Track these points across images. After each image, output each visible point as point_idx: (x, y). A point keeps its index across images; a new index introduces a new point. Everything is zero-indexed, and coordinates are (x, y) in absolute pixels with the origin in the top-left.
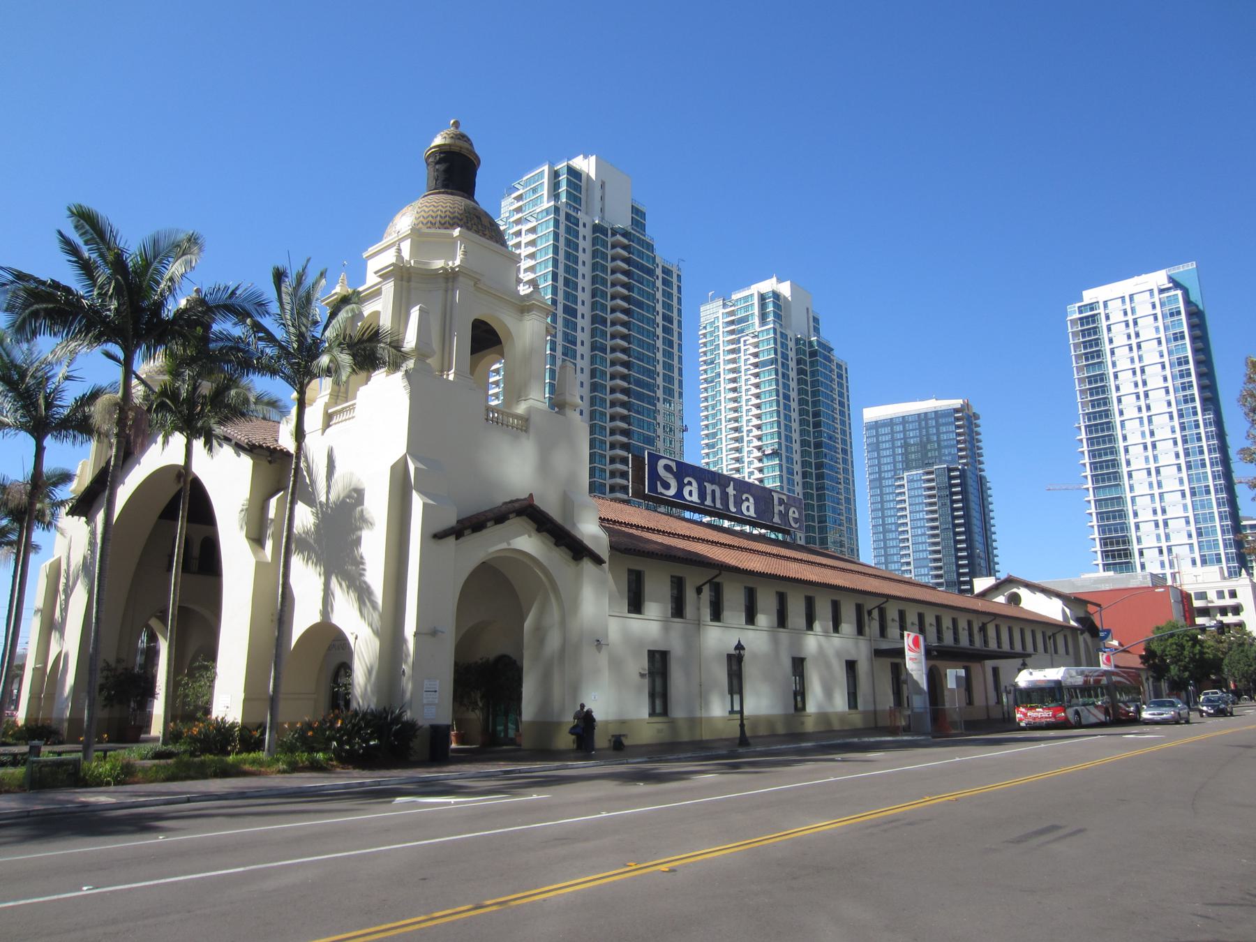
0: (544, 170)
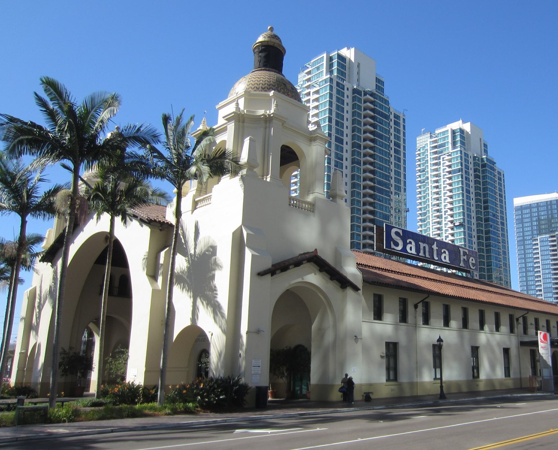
0: (323, 57)
